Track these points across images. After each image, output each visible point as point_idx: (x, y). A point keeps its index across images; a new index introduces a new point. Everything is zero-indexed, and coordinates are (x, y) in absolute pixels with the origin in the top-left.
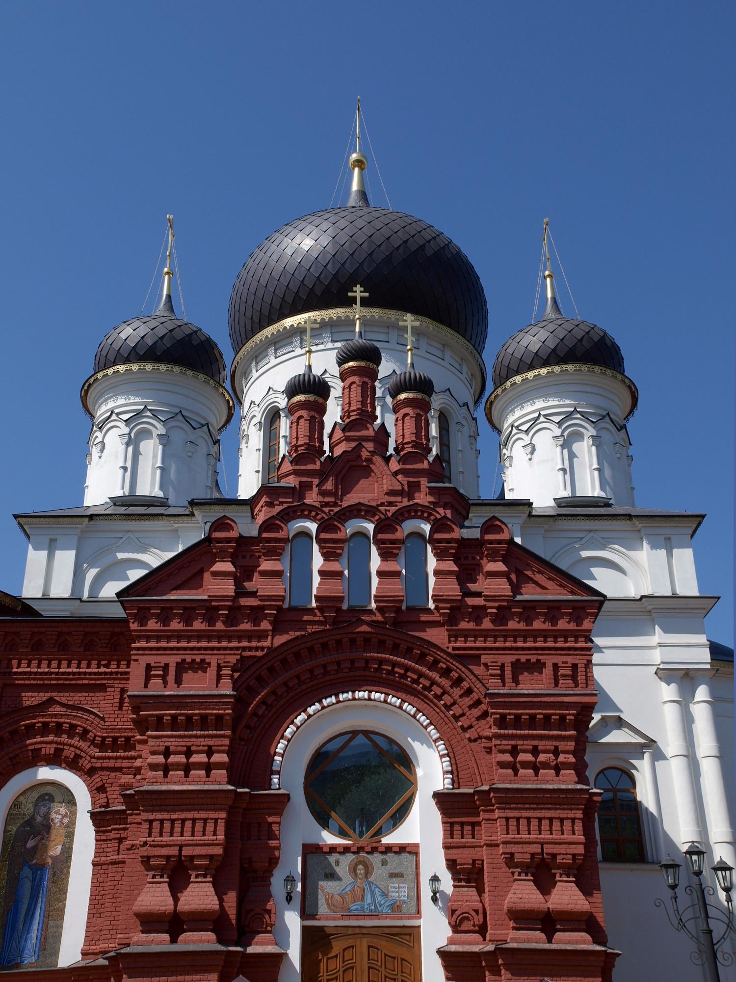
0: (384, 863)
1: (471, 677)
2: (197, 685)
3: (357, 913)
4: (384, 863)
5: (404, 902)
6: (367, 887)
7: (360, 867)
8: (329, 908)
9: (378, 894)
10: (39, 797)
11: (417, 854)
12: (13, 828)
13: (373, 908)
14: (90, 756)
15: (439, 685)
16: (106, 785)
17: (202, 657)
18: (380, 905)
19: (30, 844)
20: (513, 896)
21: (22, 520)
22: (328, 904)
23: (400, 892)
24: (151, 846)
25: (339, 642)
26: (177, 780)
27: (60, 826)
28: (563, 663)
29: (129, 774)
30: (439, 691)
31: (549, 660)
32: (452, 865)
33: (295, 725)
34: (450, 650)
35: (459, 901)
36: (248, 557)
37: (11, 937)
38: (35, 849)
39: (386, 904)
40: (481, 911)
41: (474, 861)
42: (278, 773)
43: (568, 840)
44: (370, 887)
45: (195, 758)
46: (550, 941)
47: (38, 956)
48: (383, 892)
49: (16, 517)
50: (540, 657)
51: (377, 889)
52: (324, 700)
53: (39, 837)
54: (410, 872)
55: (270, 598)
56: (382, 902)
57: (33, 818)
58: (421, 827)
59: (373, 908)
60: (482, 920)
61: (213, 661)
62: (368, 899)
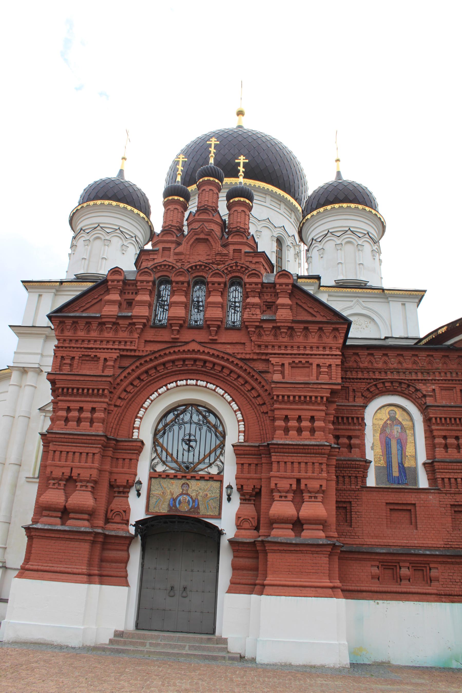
17: (95, 354)
21: (26, 284)
31: (315, 361)
36: (131, 293)
46: (63, 524)
49: (23, 282)
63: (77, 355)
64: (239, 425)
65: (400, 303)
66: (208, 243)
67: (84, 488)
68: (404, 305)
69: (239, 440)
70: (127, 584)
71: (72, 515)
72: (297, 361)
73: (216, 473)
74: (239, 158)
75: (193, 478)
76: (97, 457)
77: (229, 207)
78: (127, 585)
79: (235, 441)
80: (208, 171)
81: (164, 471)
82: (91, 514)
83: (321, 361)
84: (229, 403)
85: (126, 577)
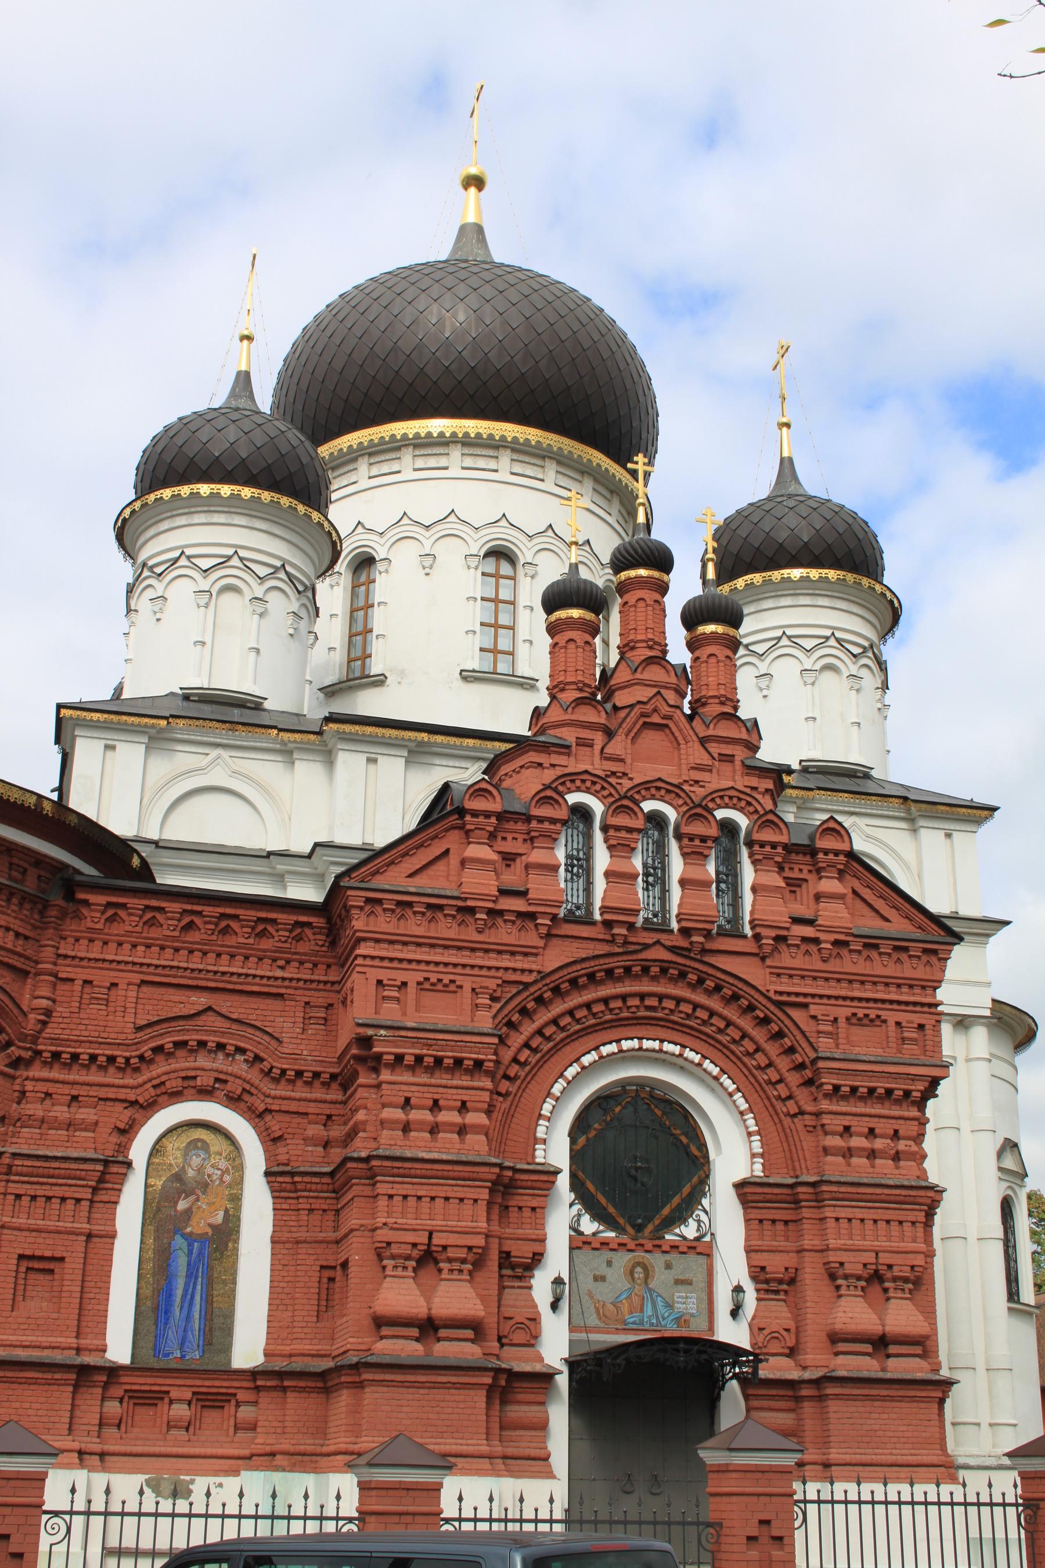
0: (668, 1266)
1: (796, 1032)
2: (443, 1013)
3: (635, 1326)
4: (668, 1266)
5: (692, 1315)
6: (647, 1295)
7: (639, 1269)
8: (600, 1319)
9: (661, 1304)
10: (189, 1143)
11: (709, 1255)
12: (158, 1183)
13: (654, 1321)
14: (264, 1094)
15: (751, 1039)
16: (286, 1136)
17: (452, 977)
18: (664, 1319)
19: (182, 1205)
20: (842, 1315)
22: (598, 1314)
23: (688, 1303)
24: (392, 1229)
25: (628, 970)
26: (423, 1144)
27: (219, 1185)
28: (908, 1022)
29: (317, 1123)
30: (751, 1048)
32: (758, 1274)
33: (565, 1079)
34: (771, 994)
35: (766, 1317)
37: (166, 1324)
38: (188, 1213)
39: (671, 1318)
40: (793, 1330)
41: (786, 1269)
42: (544, 1141)
43: (909, 1249)
44: (651, 1295)
45: (444, 1117)
47: (203, 1351)
48: (667, 1303)
50: (880, 1013)
51: (659, 1299)
52: (708, 1061)
53: (193, 1198)
54: (700, 1279)
55: (544, 903)
56: (666, 1315)
57: (183, 1169)
58: (724, 1219)
59: (654, 1321)
60: (794, 1341)
61: (467, 984)
62: (649, 1310)
63: (413, 978)
64: (750, 1142)
65: (942, 833)
66: (667, 730)
67: (455, 1276)
68: (948, 836)
69: (752, 1171)
70: (550, 1475)
71: (442, 1333)
72: (861, 1013)
73: (692, 1238)
74: (635, 459)
75: (587, 1246)
76: (482, 1206)
77: (692, 645)
78: (550, 1475)
79: (742, 1173)
80: (642, 548)
81: (594, 1234)
82: (476, 1328)
83: (902, 1017)
84: (731, 1095)
85: (546, 1458)
